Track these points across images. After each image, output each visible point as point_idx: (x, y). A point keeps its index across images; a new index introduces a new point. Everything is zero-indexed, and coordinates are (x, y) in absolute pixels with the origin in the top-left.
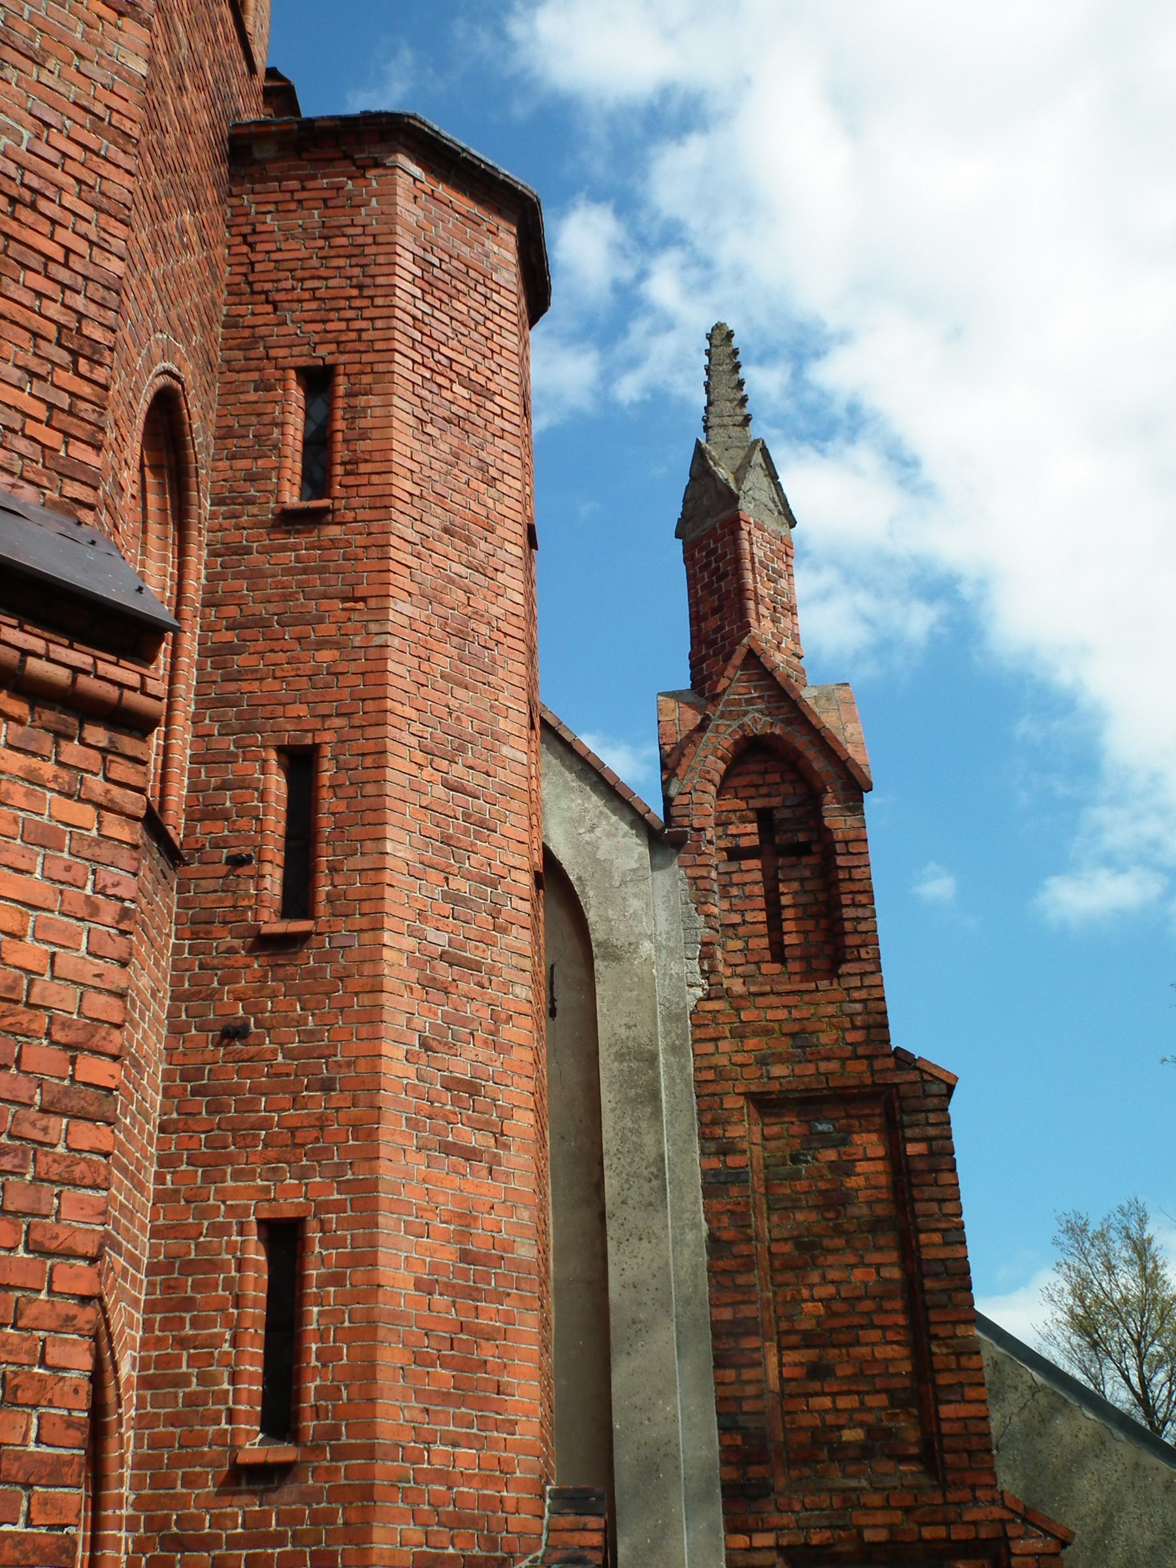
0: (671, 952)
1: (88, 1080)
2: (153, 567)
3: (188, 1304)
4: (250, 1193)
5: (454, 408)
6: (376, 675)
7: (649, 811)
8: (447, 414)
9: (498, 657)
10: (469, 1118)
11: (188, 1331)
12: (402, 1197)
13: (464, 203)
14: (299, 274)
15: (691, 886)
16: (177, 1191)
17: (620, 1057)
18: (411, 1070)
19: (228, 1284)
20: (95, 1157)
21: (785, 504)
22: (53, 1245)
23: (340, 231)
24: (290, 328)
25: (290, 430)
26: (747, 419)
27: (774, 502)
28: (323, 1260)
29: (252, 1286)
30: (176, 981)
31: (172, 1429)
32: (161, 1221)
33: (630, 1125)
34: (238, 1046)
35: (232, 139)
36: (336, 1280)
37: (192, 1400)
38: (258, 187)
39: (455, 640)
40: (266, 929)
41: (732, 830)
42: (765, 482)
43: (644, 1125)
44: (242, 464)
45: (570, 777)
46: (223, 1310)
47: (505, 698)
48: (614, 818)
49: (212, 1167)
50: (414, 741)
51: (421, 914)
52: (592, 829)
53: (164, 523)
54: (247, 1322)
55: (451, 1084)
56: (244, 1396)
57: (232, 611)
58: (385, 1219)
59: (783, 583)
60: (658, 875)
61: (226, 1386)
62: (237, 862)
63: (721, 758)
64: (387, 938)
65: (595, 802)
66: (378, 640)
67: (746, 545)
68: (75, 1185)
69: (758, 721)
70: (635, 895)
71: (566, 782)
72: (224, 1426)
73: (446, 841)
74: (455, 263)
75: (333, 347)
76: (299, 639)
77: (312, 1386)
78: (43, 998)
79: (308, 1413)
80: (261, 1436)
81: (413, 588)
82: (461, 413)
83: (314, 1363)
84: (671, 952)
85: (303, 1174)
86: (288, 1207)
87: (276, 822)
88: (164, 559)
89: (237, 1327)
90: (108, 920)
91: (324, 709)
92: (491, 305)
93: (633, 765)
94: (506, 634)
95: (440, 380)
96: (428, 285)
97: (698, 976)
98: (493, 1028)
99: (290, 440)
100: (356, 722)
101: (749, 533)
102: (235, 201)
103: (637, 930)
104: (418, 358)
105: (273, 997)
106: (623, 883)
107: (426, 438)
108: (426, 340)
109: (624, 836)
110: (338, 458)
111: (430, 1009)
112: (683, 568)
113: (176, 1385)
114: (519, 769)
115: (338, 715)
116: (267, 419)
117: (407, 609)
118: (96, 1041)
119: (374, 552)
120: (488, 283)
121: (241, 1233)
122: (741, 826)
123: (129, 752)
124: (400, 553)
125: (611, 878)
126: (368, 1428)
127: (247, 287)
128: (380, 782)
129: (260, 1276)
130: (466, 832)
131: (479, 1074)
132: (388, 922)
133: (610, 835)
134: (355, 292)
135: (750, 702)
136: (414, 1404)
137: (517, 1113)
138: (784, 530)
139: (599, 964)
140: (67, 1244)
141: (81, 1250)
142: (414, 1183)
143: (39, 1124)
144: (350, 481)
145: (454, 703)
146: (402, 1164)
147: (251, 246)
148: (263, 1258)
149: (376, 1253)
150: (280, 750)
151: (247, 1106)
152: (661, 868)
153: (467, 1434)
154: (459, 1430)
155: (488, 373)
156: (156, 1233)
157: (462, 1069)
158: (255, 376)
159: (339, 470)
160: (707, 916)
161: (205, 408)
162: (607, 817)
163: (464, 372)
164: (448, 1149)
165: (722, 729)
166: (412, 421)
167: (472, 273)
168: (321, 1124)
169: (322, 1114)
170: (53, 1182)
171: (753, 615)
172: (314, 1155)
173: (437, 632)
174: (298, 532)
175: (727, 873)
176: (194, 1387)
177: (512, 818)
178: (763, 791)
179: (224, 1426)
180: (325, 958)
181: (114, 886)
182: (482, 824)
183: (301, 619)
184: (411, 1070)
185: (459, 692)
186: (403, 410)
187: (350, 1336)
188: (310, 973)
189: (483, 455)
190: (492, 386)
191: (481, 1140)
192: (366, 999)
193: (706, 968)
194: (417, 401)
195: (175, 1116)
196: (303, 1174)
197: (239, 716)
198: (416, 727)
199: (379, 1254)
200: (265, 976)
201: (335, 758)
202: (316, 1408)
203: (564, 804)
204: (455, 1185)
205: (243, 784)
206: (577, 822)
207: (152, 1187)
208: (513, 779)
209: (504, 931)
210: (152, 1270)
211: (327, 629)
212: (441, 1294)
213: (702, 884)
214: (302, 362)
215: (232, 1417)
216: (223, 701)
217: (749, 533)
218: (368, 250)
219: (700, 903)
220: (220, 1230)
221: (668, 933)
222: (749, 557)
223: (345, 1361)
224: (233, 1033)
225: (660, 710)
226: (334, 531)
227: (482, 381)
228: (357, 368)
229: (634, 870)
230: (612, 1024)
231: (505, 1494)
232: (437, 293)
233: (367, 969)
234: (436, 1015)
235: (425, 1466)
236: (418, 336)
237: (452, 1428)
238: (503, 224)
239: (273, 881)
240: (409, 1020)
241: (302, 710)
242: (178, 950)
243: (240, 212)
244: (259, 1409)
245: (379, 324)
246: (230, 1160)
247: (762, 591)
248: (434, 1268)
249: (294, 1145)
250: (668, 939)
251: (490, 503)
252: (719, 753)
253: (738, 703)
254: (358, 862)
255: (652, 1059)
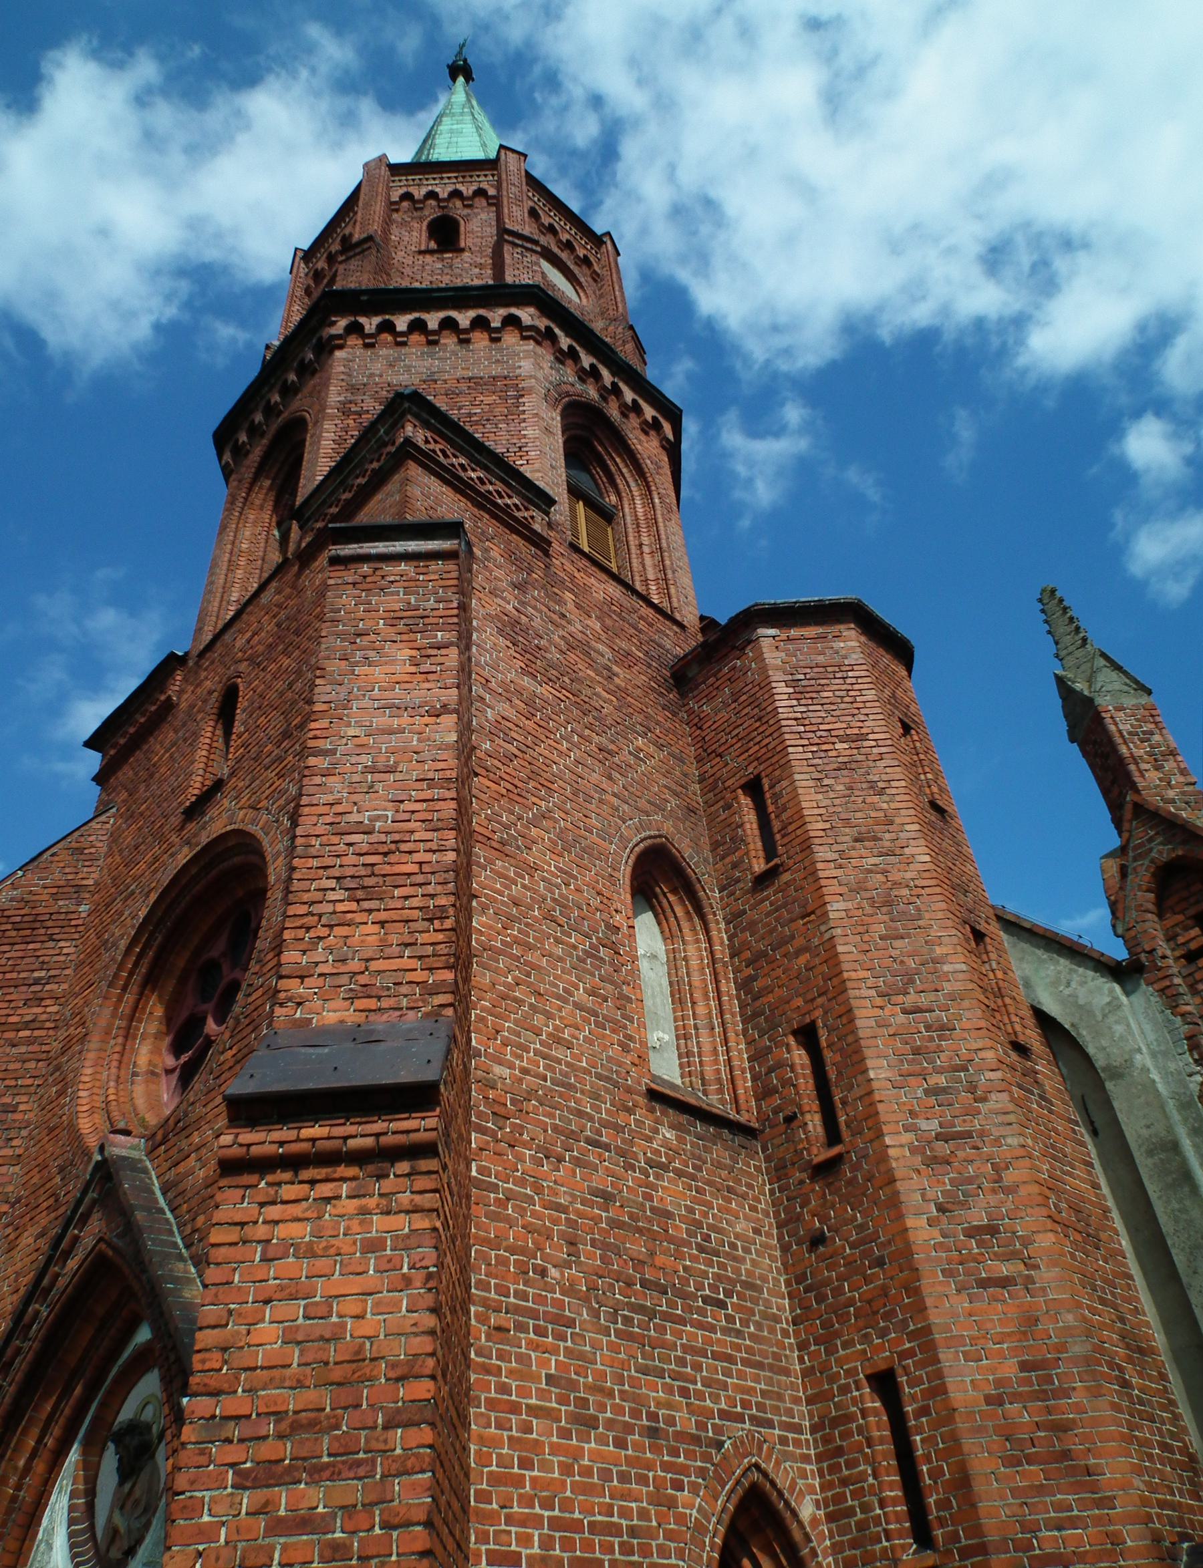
0: (1165, 1054)
1: (412, 1398)
2: (691, 950)
3: (839, 1451)
4: (856, 1356)
5: (840, 760)
6: (832, 958)
7: (1103, 954)
8: (835, 766)
9: (923, 907)
10: (995, 1254)
11: (846, 1472)
12: (955, 1333)
13: (811, 631)
14: (727, 730)
15: (1161, 996)
16: (813, 1367)
17: (1150, 1153)
18: (935, 1232)
19: (860, 1430)
20: (421, 1450)
21: (1136, 682)
22: (396, 1521)
23: (740, 692)
24: (732, 765)
25: (748, 826)
26: (1084, 640)
27: (1126, 684)
28: (913, 1397)
29: (875, 1428)
30: (777, 1214)
31: (854, 1552)
32: (809, 1392)
33: (1177, 1206)
34: (822, 1249)
35: (673, 676)
36: (924, 1411)
37: (862, 1526)
38: (696, 693)
39: (884, 909)
40: (816, 1160)
41: (1181, 940)
42: (1114, 675)
43: (1188, 1203)
44: (728, 860)
45: (1039, 952)
46: (861, 1451)
47: (935, 932)
48: (1081, 970)
49: (827, 1340)
50: (873, 992)
51: (913, 1114)
52: (1068, 985)
53: (690, 919)
54: (879, 1458)
55: (971, 1232)
56: (892, 1517)
57: (748, 954)
58: (945, 1355)
59: (1157, 738)
60: (1133, 998)
61: (878, 1511)
62: (789, 1119)
63: (1148, 891)
64: (888, 1140)
65: (1064, 963)
66: (827, 936)
67: (1113, 728)
68: (409, 1474)
69: (1162, 852)
70: (1117, 1022)
71: (1039, 958)
72: (885, 1544)
73: (916, 1051)
74: (816, 670)
75: (755, 763)
76: (785, 956)
77: (931, 1500)
78: (379, 1352)
79: (935, 1524)
80: (915, 1546)
81: (844, 890)
82: (846, 759)
83: (928, 1482)
84: (1165, 1054)
85: (883, 1333)
86: (881, 1360)
87: (806, 1084)
88: (697, 941)
89: (872, 1461)
90: (418, 1284)
91: (810, 997)
92: (849, 681)
93: (1091, 924)
94: (923, 887)
95: (824, 747)
96: (799, 692)
97: (1193, 1066)
98: (996, 1177)
99: (749, 832)
100: (830, 996)
101: (1112, 717)
102: (687, 708)
103: (1127, 1049)
104: (806, 742)
105: (833, 1207)
106: (1105, 1016)
107: (825, 789)
108: (808, 728)
109: (1093, 980)
110: (775, 830)
111: (938, 1181)
112: (1084, 761)
113: (848, 1517)
114: (961, 976)
115: (819, 996)
116: (733, 826)
117: (841, 905)
118: (416, 1370)
119: (810, 879)
120: (843, 668)
121: (857, 1390)
122: (1186, 934)
123: (424, 1169)
124: (826, 871)
125: (1094, 1016)
126: (976, 1530)
127: (707, 753)
128: (854, 1031)
129: (881, 1419)
130: (931, 1039)
131: (994, 1217)
132: (885, 1129)
133: (1083, 983)
134: (758, 724)
135: (1151, 840)
136: (1012, 1501)
137: (1038, 1237)
138: (1144, 700)
139: (1109, 1085)
140: (405, 1518)
141: (415, 1519)
142: (962, 1319)
143: (381, 1438)
144: (786, 840)
145: (894, 953)
146: (948, 1306)
147: (700, 728)
148: (878, 1404)
149: (944, 1384)
150: (795, 1033)
151: (838, 1291)
152: (1133, 992)
153: (1068, 1517)
154: (1060, 1515)
155: (860, 724)
156: (810, 1401)
157: (979, 1217)
158: (721, 803)
159: (778, 837)
160: (1182, 1015)
161: (695, 843)
162: (1076, 971)
163: (841, 733)
164: (983, 1284)
165: (1139, 869)
166: (811, 783)
167: (829, 669)
168: (884, 1291)
169: (883, 1285)
170: (394, 1476)
171: (1136, 774)
172: (888, 1316)
173: (869, 910)
174: (767, 887)
175: (1189, 975)
176: (859, 1516)
177: (968, 1014)
178: (1192, 900)
179: (885, 1544)
180: (855, 1168)
181: (420, 1261)
182: (943, 1028)
183: (784, 942)
184: (935, 1232)
185: (898, 943)
186: (803, 780)
187: (943, 1455)
188: (850, 1182)
189: (870, 778)
190: (864, 731)
191: (1012, 1268)
192: (888, 1190)
193: (1196, 1057)
194: (812, 769)
195: (799, 1311)
196: (883, 1333)
197: (766, 1020)
198: (870, 982)
199: (948, 1385)
200: (824, 1194)
201: (825, 1025)
202: (938, 1518)
203: (1043, 974)
204: (1000, 1313)
205: (780, 1065)
206: (1055, 983)
207: (798, 1368)
208: (959, 986)
209: (984, 1100)
210: (814, 1429)
211: (799, 942)
212: (1011, 1403)
213: (1169, 992)
214: (743, 781)
215: (888, 1535)
216: (756, 1015)
217: (1112, 717)
218: (758, 695)
219: (1174, 1008)
220: (844, 1390)
221: (1157, 1040)
222: (1117, 735)
223: (947, 1476)
224: (817, 1240)
225: (1103, 871)
226: (786, 877)
227: (856, 731)
228: (771, 769)
229: (1109, 1004)
230: (1134, 1129)
231: (1122, 1563)
232: (808, 696)
233: (883, 1168)
234: (944, 1183)
235: (1037, 1552)
236: (802, 729)
237: (1052, 1514)
238: (842, 627)
239: (814, 1123)
240: (923, 1195)
241: (799, 1002)
242: (772, 1192)
243: (690, 712)
244: (908, 1524)
245: (775, 735)
246: (838, 1335)
247: (1138, 752)
248: (999, 1383)
249: (873, 1312)
250: (1159, 1045)
251: (885, 806)
252: (1144, 888)
253: (1141, 845)
254: (857, 1092)
255: (1174, 1147)
